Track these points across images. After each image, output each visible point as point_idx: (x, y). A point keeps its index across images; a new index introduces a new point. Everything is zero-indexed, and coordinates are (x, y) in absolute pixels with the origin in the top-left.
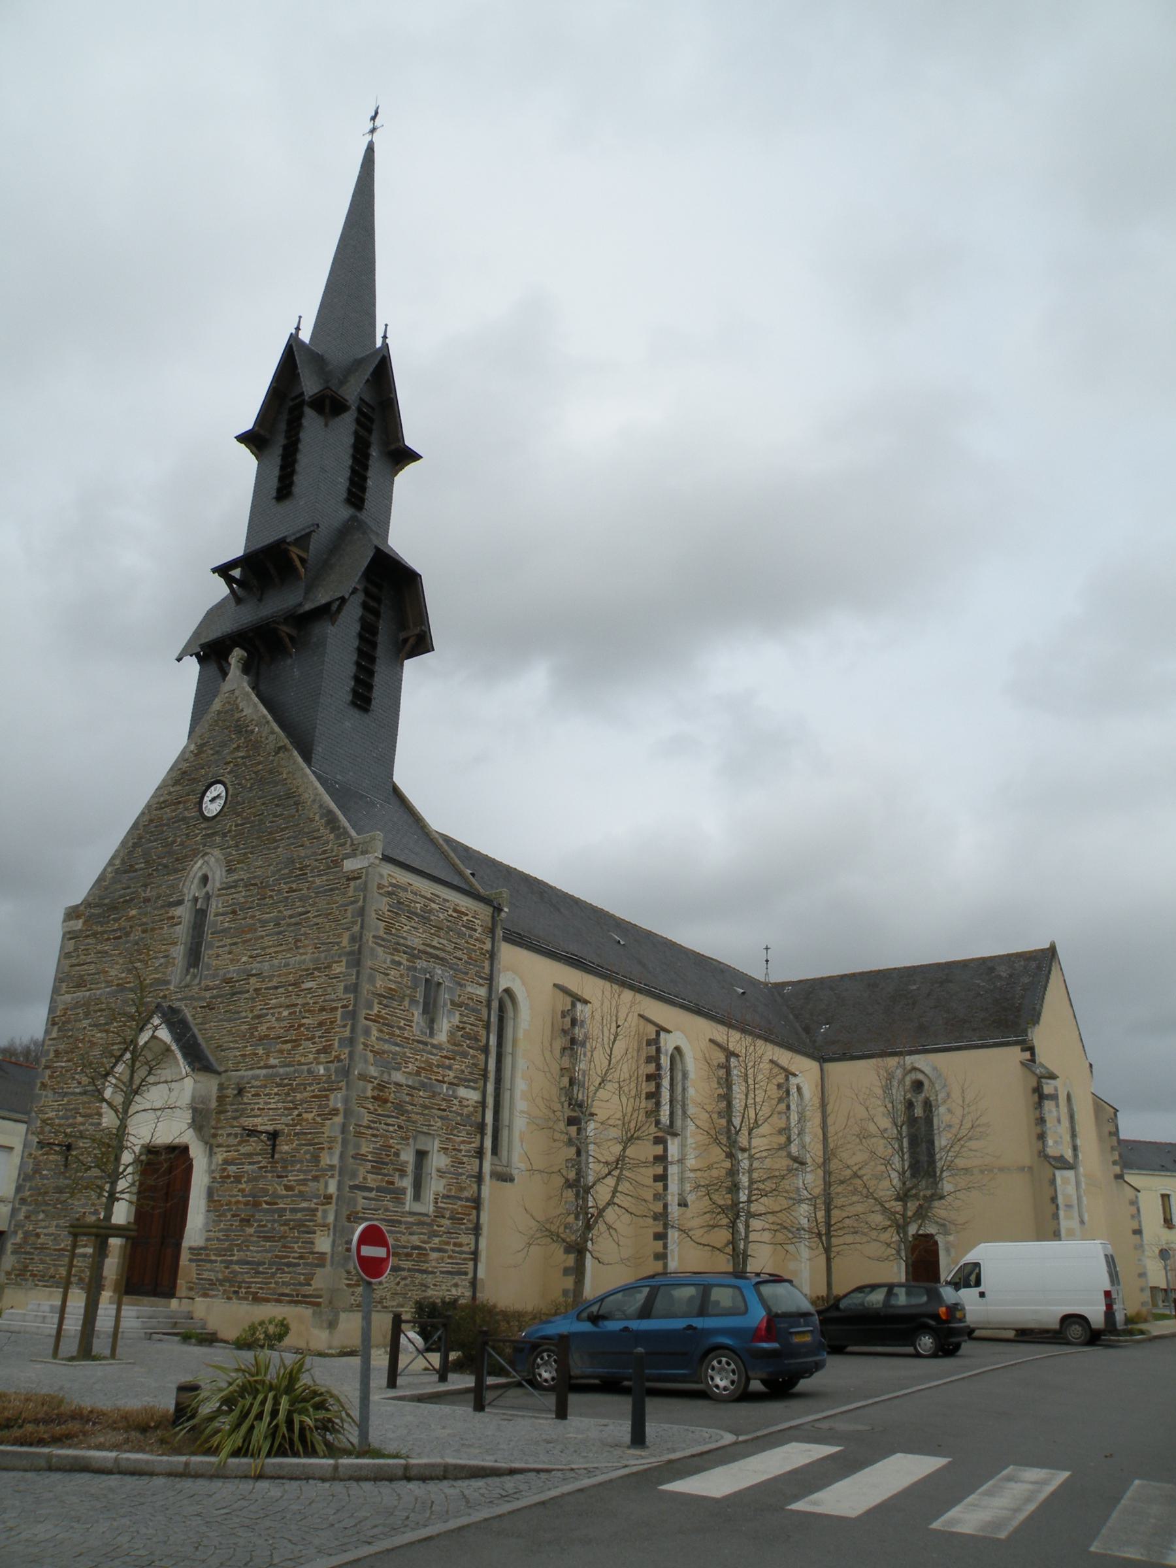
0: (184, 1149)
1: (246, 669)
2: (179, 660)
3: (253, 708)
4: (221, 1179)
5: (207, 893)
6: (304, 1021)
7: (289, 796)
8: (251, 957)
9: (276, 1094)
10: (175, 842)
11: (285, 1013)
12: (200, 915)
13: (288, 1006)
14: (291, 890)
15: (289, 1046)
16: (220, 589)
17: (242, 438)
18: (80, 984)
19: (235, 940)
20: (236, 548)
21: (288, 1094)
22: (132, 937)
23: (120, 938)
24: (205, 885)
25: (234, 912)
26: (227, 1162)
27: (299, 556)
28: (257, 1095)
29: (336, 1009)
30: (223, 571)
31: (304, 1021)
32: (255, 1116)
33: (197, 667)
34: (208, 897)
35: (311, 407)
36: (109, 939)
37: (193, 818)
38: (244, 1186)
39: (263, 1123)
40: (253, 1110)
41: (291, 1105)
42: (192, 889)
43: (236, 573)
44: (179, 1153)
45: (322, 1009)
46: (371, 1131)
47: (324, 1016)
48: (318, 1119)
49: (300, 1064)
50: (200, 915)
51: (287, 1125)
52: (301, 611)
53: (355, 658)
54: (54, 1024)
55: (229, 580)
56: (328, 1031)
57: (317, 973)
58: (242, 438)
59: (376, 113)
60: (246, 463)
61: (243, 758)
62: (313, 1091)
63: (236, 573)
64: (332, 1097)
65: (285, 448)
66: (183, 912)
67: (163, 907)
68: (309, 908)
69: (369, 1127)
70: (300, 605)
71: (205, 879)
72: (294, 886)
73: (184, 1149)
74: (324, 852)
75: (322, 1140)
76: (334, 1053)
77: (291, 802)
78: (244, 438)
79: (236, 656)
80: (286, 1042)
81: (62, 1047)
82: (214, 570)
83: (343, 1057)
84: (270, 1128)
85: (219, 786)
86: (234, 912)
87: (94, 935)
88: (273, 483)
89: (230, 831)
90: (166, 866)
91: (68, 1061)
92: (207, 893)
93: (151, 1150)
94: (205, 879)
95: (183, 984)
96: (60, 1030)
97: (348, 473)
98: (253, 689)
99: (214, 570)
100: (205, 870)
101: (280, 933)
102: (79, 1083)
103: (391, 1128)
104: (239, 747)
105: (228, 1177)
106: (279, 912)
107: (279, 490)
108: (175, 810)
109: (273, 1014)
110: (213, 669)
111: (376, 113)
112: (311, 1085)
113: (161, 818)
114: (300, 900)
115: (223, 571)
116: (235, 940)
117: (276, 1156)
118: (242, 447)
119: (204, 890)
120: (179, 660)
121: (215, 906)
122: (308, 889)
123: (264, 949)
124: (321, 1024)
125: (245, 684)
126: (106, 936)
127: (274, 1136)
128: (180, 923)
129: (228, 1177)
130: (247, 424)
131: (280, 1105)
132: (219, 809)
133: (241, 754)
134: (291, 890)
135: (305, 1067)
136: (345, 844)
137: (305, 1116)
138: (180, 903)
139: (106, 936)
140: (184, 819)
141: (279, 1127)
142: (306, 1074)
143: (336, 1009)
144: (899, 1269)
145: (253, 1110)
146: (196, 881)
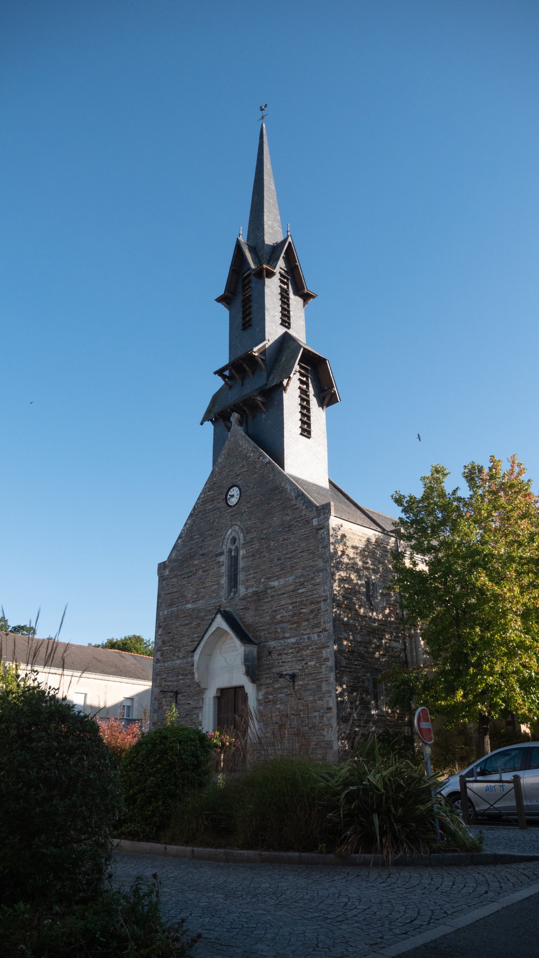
0: (242, 687)
1: (241, 423)
2: (202, 424)
3: (246, 444)
4: (263, 702)
5: (236, 547)
6: (303, 611)
7: (276, 488)
8: (266, 579)
9: (291, 653)
10: (214, 521)
11: (290, 608)
12: (234, 560)
13: (291, 604)
14: (285, 540)
15: (295, 626)
16: (219, 382)
17: (219, 300)
18: (171, 605)
19: (256, 570)
20: (224, 360)
21: (298, 652)
22: (198, 575)
23: (191, 576)
24: (235, 543)
25: (253, 555)
26: (267, 693)
27: (261, 358)
28: (280, 654)
29: (320, 602)
30: (220, 372)
31: (303, 611)
32: (281, 666)
33: (212, 427)
34: (237, 550)
35: (254, 276)
36: (185, 578)
37: (223, 507)
38: (279, 706)
39: (287, 669)
40: (279, 663)
41: (300, 658)
42: (227, 545)
43: (227, 373)
44: (239, 690)
45: (312, 603)
46: (348, 670)
47: (313, 607)
48: (318, 665)
49: (303, 634)
50: (234, 560)
51: (299, 670)
52: (267, 388)
53: (299, 410)
54: (160, 627)
55: (224, 377)
56: (316, 615)
57: (306, 584)
58: (219, 300)
59: (419, 436)
60: (223, 313)
61: (246, 471)
62: (312, 649)
63: (227, 373)
64: (324, 652)
65: (243, 301)
66: (223, 559)
67: (212, 557)
68: (296, 548)
69: (346, 667)
70: (266, 384)
71: (234, 540)
72: (286, 537)
73: (242, 687)
74: (300, 517)
75: (321, 676)
76: (322, 627)
77: (277, 492)
78: (220, 300)
79: (235, 417)
80: (293, 624)
81: (166, 638)
82: (215, 373)
83: (327, 628)
84: (290, 672)
85: (235, 488)
86: (253, 555)
87: (176, 576)
88: (239, 321)
89: (245, 512)
90: (211, 535)
91: (171, 646)
92: (236, 547)
93: (223, 692)
94: (234, 540)
95: (229, 598)
96: (163, 629)
97: (280, 309)
98: (246, 433)
99: (215, 373)
100: (234, 534)
101: (281, 563)
102: (178, 657)
103: (358, 667)
104: (243, 466)
105: (269, 701)
106: (279, 552)
107: (244, 325)
108: (212, 504)
109: (283, 609)
110: (221, 422)
111: (419, 436)
112: (311, 645)
113: (205, 510)
114: (291, 544)
115: (220, 372)
116: (256, 570)
117: (296, 688)
118: (220, 304)
119: (235, 545)
120: (202, 424)
121: (242, 552)
122: (295, 537)
123: (274, 573)
124: (312, 611)
125: (242, 431)
126: (183, 576)
127: (293, 677)
128: (223, 565)
129: (269, 701)
130: (221, 291)
131: (294, 659)
132: (237, 500)
133: (245, 469)
134: (285, 540)
135: (306, 636)
136: (312, 510)
137: (309, 663)
138: (222, 554)
139: (183, 576)
140: (218, 508)
141: (295, 671)
142: (306, 640)
143: (320, 602)
144: (317, 502)
145: (279, 663)
146: (229, 541)
